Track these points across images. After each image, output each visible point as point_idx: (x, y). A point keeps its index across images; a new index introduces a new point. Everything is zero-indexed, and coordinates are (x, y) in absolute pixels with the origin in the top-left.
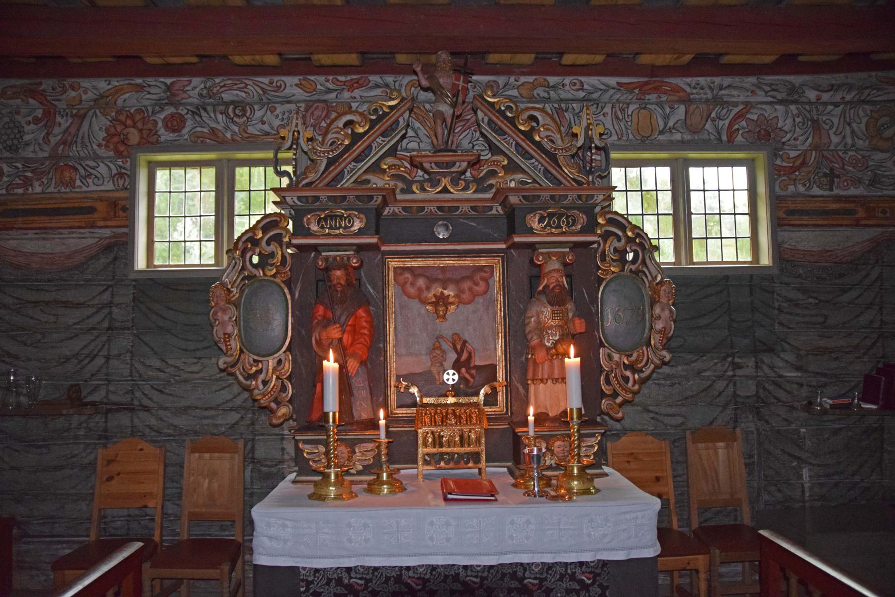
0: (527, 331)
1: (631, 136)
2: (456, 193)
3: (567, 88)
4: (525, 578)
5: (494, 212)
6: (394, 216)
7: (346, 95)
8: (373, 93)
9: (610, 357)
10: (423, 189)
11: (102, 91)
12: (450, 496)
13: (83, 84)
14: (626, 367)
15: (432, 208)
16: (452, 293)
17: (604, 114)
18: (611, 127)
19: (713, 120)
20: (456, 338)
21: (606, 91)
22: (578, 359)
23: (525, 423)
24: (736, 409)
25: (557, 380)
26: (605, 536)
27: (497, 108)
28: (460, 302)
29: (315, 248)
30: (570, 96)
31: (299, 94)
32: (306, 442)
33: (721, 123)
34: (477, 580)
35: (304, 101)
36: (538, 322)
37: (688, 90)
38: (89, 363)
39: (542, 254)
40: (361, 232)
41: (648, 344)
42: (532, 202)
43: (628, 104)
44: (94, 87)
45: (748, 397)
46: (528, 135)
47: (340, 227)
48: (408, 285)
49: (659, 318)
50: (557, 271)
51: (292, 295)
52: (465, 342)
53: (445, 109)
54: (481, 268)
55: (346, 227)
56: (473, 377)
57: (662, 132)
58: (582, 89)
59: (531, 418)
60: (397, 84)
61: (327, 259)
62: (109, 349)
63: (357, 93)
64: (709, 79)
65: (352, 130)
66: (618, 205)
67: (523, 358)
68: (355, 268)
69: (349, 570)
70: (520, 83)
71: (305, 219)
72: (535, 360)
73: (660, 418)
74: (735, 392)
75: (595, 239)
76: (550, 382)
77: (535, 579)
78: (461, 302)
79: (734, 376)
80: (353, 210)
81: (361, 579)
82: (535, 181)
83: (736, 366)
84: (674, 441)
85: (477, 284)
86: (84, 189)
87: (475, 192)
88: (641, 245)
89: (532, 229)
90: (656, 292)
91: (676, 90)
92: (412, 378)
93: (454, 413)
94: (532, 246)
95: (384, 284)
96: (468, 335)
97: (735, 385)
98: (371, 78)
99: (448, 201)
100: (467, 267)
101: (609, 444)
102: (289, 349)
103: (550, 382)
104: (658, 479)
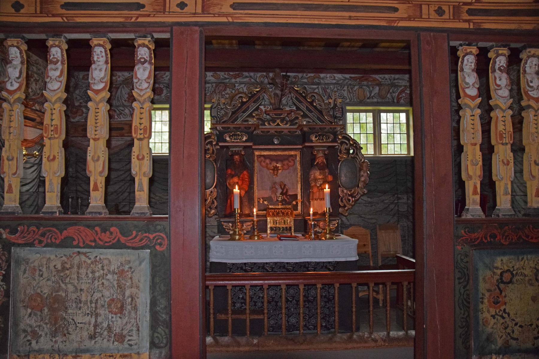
0: (310, 180)
1: (355, 100)
2: (282, 126)
3: (328, 79)
4: (309, 297)
5: (297, 133)
6: (257, 135)
7: (233, 80)
8: (245, 80)
9: (343, 191)
10: (269, 124)
11: (126, 77)
12: (282, 238)
13: (118, 74)
14: (349, 195)
15: (272, 131)
16: (280, 166)
17: (344, 90)
18: (347, 96)
19: (391, 93)
20: (281, 183)
21: (344, 80)
22: (329, 190)
23: (309, 215)
24: (398, 217)
25: (321, 199)
26: (338, 252)
27: (299, 92)
28: (283, 169)
29: (227, 147)
30: (329, 82)
31: (213, 79)
32: (224, 222)
33: (394, 94)
34: (292, 268)
35: (215, 83)
36: (314, 177)
37: (380, 80)
38: (121, 195)
39: (316, 150)
40: (246, 141)
41: (358, 186)
42: (312, 130)
43: (354, 86)
44: (123, 75)
45: (404, 212)
46: (311, 103)
47: (238, 139)
48: (262, 162)
49: (363, 176)
50: (322, 157)
51: (217, 165)
52: (285, 185)
53: (278, 92)
54: (292, 156)
55: (240, 139)
56: (288, 199)
57: (368, 98)
58: (335, 79)
59: (311, 212)
60: (255, 76)
61: (232, 151)
62: (130, 189)
63: (238, 80)
64: (389, 75)
65: (242, 100)
66: (349, 131)
67: (308, 192)
68: (242, 155)
69: (245, 264)
70: (308, 76)
71: (224, 136)
72: (313, 192)
73: (366, 220)
74: (398, 210)
75: (337, 144)
76: (319, 200)
77: (312, 268)
78: (283, 169)
79: (397, 203)
80: (244, 132)
81: (249, 267)
82: (314, 121)
83: (399, 198)
84: (372, 230)
85: (290, 162)
86: (119, 119)
87: (290, 125)
88: (356, 147)
89: (312, 140)
90: (362, 166)
91: (375, 80)
92: (264, 199)
93: (281, 212)
94: (312, 147)
95: (254, 161)
96: (287, 182)
97: (398, 207)
98: (244, 73)
99: (279, 129)
100: (286, 155)
101: (344, 230)
102: (215, 187)
103: (319, 200)
104: (365, 245)
